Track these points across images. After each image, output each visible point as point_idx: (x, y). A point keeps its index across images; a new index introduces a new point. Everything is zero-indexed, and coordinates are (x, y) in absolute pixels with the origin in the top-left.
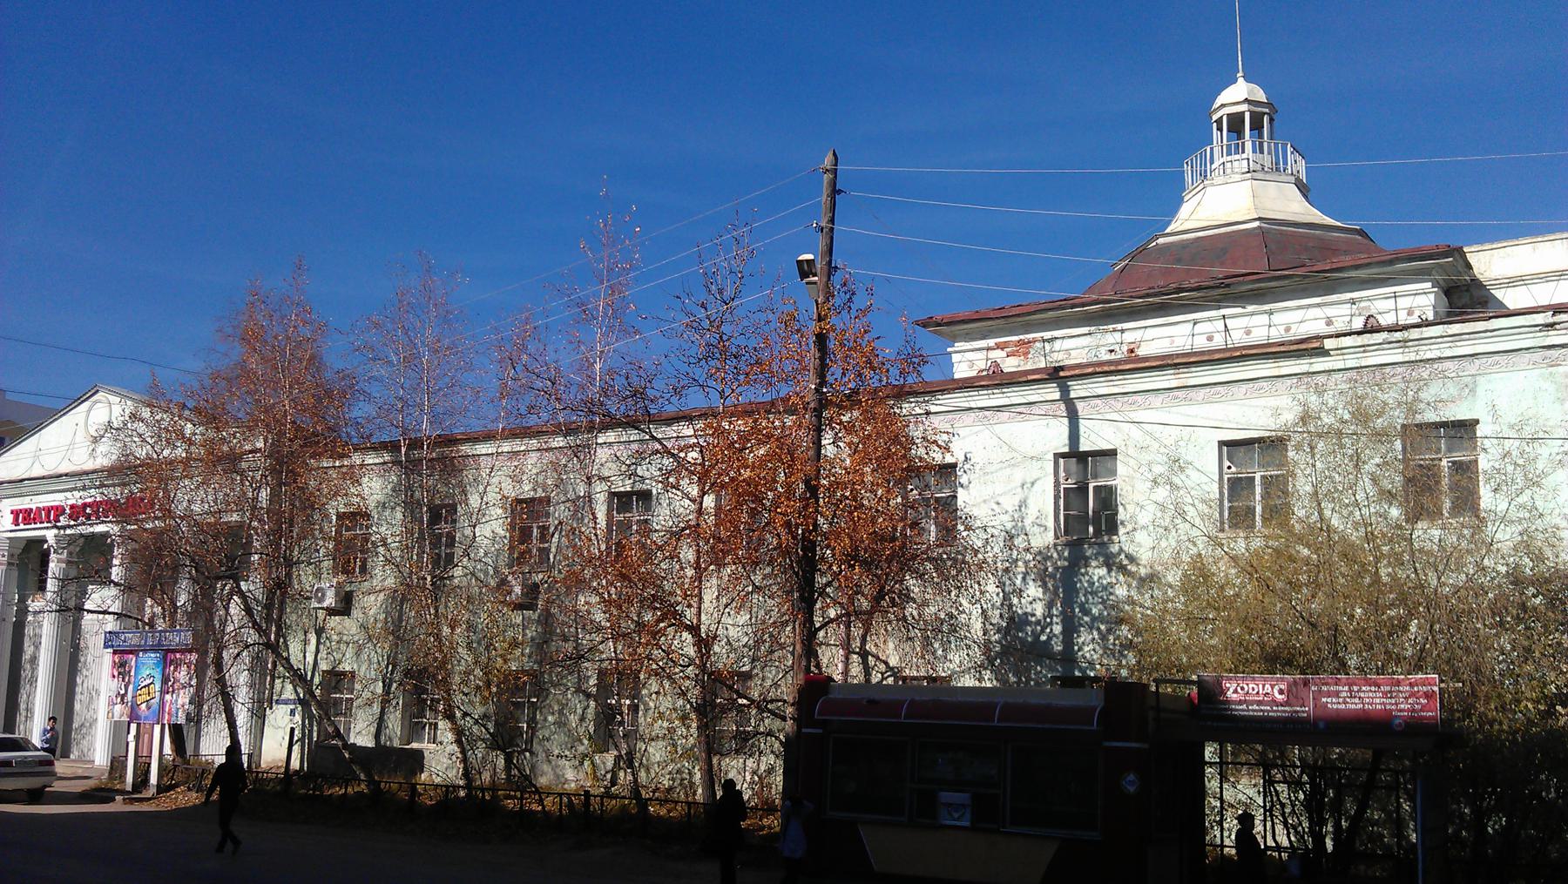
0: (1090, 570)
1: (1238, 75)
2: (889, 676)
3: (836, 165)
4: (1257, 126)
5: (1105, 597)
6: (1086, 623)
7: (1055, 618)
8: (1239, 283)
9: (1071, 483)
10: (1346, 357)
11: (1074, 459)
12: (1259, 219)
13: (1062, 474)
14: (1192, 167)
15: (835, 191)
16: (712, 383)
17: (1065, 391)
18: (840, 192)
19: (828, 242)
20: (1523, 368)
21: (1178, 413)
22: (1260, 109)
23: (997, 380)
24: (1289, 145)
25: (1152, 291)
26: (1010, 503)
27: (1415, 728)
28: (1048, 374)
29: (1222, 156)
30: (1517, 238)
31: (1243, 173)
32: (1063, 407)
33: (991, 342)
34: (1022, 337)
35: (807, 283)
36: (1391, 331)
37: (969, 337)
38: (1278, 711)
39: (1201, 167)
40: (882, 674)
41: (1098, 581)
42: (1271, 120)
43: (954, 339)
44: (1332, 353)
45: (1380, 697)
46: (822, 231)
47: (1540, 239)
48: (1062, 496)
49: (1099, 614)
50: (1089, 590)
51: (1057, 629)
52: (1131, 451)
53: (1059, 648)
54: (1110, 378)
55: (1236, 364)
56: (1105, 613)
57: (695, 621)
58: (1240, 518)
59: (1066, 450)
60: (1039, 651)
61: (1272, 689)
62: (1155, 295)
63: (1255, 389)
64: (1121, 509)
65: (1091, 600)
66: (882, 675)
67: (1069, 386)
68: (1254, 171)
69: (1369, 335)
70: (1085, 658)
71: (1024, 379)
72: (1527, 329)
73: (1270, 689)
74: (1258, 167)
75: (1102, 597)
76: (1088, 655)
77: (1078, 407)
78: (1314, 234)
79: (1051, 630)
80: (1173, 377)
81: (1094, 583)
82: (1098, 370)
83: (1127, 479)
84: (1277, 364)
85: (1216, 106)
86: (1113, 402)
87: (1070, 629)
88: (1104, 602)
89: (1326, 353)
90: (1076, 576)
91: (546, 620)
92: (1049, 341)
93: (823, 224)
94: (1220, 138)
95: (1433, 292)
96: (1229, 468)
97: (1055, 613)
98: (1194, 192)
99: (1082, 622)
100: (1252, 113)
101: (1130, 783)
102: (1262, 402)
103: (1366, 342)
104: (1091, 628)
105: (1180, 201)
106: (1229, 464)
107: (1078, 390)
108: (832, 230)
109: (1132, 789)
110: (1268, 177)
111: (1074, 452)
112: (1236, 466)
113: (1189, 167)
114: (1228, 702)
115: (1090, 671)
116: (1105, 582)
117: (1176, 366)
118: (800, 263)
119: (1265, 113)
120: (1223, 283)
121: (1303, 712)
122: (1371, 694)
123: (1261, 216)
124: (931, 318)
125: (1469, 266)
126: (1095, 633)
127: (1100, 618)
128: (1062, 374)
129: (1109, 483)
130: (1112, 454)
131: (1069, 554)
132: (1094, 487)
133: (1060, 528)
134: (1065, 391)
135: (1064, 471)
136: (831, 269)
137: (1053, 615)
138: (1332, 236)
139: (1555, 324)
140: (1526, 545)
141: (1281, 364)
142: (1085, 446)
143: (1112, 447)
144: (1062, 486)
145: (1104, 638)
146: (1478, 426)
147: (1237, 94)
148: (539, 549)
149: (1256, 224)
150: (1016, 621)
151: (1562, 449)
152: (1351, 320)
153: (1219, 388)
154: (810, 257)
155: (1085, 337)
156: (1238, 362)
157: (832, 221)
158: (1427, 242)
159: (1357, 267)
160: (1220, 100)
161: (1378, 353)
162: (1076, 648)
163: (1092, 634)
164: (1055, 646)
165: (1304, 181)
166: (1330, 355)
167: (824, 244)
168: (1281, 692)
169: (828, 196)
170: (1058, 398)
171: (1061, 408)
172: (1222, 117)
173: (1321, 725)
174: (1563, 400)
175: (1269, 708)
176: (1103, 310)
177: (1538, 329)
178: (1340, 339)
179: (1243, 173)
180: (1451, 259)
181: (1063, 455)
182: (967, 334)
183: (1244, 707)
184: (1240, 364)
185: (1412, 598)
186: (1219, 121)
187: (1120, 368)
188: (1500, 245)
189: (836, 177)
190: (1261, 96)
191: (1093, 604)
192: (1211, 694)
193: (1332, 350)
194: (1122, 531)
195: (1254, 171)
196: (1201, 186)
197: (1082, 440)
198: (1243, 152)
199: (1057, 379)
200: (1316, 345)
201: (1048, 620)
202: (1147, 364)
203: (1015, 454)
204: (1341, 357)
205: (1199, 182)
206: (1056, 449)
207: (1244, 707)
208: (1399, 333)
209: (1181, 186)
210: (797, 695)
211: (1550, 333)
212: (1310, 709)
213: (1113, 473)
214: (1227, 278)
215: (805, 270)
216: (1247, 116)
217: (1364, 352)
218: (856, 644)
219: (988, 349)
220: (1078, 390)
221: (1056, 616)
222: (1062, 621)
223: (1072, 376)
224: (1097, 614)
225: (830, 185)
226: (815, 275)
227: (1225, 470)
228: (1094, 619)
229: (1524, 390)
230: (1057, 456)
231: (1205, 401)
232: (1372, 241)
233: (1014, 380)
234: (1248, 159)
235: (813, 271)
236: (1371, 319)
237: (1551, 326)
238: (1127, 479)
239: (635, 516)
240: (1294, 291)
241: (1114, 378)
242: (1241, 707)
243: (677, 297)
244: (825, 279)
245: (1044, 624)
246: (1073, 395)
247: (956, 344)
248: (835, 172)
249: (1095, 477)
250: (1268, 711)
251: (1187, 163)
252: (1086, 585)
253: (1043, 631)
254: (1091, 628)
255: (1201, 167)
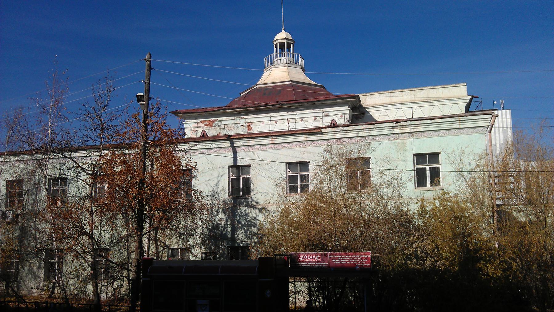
0: (241, 208)
1: (282, 29)
2: (166, 248)
3: (151, 58)
4: (289, 47)
5: (246, 218)
6: (240, 227)
7: (228, 225)
8: (287, 104)
9: (234, 177)
10: (328, 135)
11: (235, 168)
12: (291, 81)
13: (231, 173)
14: (267, 61)
15: (150, 69)
16: (97, 139)
17: (232, 144)
18: (152, 69)
19: (148, 88)
20: (385, 140)
21: (272, 153)
22: (290, 42)
23: (205, 138)
24: (299, 55)
25: (257, 105)
26: (213, 183)
27: (363, 269)
28: (227, 138)
29: (277, 57)
30: (374, 92)
31: (285, 64)
32: (231, 149)
33: (199, 120)
34: (210, 119)
35: (140, 104)
36: (343, 127)
37: (191, 118)
38: (318, 265)
39: (270, 62)
40: (163, 247)
41: (244, 212)
42: (293, 46)
43: (185, 119)
44: (324, 133)
45: (352, 259)
46: (145, 84)
47: (382, 93)
48: (231, 181)
49: (244, 223)
50: (241, 215)
51: (229, 229)
52: (256, 166)
53: (230, 236)
54: (249, 140)
55: (292, 136)
56: (246, 223)
57: (91, 233)
58: (293, 189)
59: (232, 165)
60: (223, 237)
61: (316, 257)
62: (258, 107)
63: (298, 145)
64: (252, 185)
65: (241, 219)
66: (163, 248)
67: (234, 142)
68: (288, 63)
69: (336, 128)
70: (239, 239)
71: (218, 139)
72: (387, 128)
73: (315, 257)
74: (289, 62)
75: (245, 218)
76: (240, 238)
77: (237, 149)
78: (308, 87)
79: (227, 230)
80: (271, 140)
81: (242, 212)
82: (244, 136)
83: (254, 176)
84: (306, 137)
85: (275, 39)
86: (249, 148)
87: (234, 230)
88: (246, 220)
89: (322, 133)
90: (236, 210)
91: (22, 229)
92: (220, 121)
93: (146, 81)
94: (276, 51)
95: (349, 110)
96: (289, 172)
97: (228, 223)
98: (268, 70)
99: (238, 227)
100: (287, 43)
101: (268, 293)
102: (300, 149)
103: (335, 130)
104: (242, 229)
105: (262, 73)
106: (289, 170)
107: (237, 143)
108: (149, 83)
109: (269, 296)
110: (293, 66)
111: (235, 166)
112: (291, 171)
113: (266, 60)
114: (300, 262)
115: (241, 244)
116: (246, 212)
117: (272, 136)
118: (137, 96)
119: (291, 43)
120: (281, 104)
121: (326, 265)
122: (349, 258)
123: (292, 80)
124: (177, 111)
125: (360, 101)
126: (243, 230)
127: (245, 225)
128: (231, 137)
129: (247, 177)
130: (249, 166)
131: (233, 202)
132: (242, 178)
133: (230, 193)
134: (232, 144)
135: (232, 172)
136: (149, 98)
137: (228, 224)
138: (314, 88)
139: (396, 126)
140: (397, 208)
141: (307, 137)
142: (239, 163)
143: (249, 164)
144: (231, 178)
145: (246, 232)
146: (370, 159)
147: (282, 36)
148: (19, 201)
149: (290, 82)
150: (216, 227)
151: (411, 175)
152: (322, 118)
153: (286, 144)
154: (142, 94)
155: (233, 120)
156: (293, 136)
157: (149, 80)
158: (348, 93)
159: (325, 100)
160: (277, 37)
161: (339, 134)
162: (236, 236)
163: (242, 231)
164: (228, 235)
165: (304, 67)
166: (323, 134)
167: (146, 88)
168: (319, 258)
169: (148, 70)
170: (230, 146)
171: (231, 149)
172: (277, 43)
173: (332, 269)
174: (398, 151)
175: (314, 264)
176: (239, 111)
177: (390, 128)
178: (327, 129)
179: (285, 64)
180: (355, 99)
181: (231, 167)
182: (190, 117)
183: (306, 264)
184: (293, 136)
185: (357, 221)
186: (276, 45)
187: (252, 136)
188: (369, 94)
189: (151, 63)
190: (290, 37)
191: (242, 220)
192: (295, 259)
193: (324, 133)
194: (252, 194)
195: (288, 63)
196: (271, 67)
197: (238, 161)
198: (284, 57)
199: (230, 139)
200: (319, 131)
201: (226, 226)
202: (262, 135)
203: (214, 166)
204: (327, 135)
205: (270, 66)
206: (229, 164)
207: (306, 264)
208: (346, 128)
209: (263, 67)
210: (137, 263)
211: (395, 129)
212: (328, 264)
213: (249, 173)
214: (282, 102)
215: (140, 99)
216: (286, 44)
217: (335, 133)
218: (152, 237)
219: (198, 123)
220: (237, 143)
221: (229, 224)
222: (231, 226)
223: (235, 138)
224: (243, 224)
225: (149, 67)
226: (143, 101)
227: (288, 173)
228: (242, 225)
229: (385, 148)
230: (229, 167)
231: (281, 149)
232: (326, 89)
233: (214, 139)
234: (286, 59)
235: (143, 99)
236: (334, 121)
237: (395, 127)
238: (254, 176)
239: (60, 187)
240: (304, 107)
241: (250, 139)
242: (305, 264)
243: (84, 105)
244: (147, 102)
245: (225, 228)
246: (235, 145)
247: (186, 121)
248: (150, 61)
249: (243, 174)
250: (314, 265)
251: (265, 59)
252: (240, 213)
253: (224, 230)
254: (242, 229)
255: (270, 62)
